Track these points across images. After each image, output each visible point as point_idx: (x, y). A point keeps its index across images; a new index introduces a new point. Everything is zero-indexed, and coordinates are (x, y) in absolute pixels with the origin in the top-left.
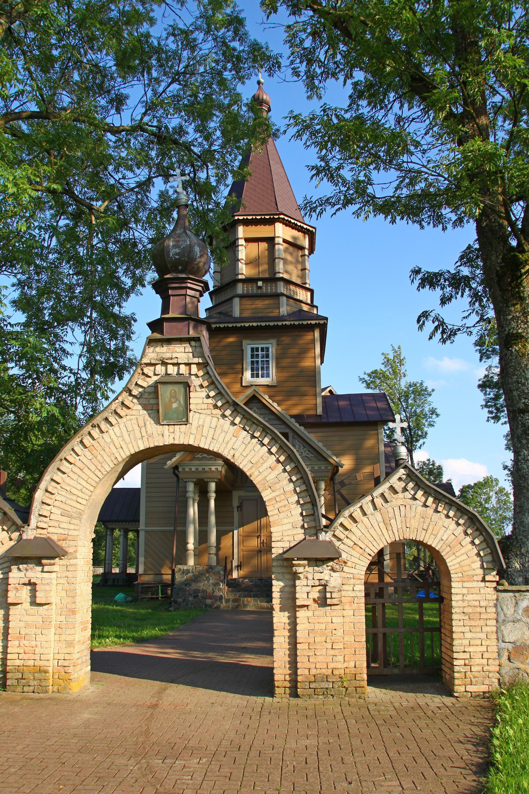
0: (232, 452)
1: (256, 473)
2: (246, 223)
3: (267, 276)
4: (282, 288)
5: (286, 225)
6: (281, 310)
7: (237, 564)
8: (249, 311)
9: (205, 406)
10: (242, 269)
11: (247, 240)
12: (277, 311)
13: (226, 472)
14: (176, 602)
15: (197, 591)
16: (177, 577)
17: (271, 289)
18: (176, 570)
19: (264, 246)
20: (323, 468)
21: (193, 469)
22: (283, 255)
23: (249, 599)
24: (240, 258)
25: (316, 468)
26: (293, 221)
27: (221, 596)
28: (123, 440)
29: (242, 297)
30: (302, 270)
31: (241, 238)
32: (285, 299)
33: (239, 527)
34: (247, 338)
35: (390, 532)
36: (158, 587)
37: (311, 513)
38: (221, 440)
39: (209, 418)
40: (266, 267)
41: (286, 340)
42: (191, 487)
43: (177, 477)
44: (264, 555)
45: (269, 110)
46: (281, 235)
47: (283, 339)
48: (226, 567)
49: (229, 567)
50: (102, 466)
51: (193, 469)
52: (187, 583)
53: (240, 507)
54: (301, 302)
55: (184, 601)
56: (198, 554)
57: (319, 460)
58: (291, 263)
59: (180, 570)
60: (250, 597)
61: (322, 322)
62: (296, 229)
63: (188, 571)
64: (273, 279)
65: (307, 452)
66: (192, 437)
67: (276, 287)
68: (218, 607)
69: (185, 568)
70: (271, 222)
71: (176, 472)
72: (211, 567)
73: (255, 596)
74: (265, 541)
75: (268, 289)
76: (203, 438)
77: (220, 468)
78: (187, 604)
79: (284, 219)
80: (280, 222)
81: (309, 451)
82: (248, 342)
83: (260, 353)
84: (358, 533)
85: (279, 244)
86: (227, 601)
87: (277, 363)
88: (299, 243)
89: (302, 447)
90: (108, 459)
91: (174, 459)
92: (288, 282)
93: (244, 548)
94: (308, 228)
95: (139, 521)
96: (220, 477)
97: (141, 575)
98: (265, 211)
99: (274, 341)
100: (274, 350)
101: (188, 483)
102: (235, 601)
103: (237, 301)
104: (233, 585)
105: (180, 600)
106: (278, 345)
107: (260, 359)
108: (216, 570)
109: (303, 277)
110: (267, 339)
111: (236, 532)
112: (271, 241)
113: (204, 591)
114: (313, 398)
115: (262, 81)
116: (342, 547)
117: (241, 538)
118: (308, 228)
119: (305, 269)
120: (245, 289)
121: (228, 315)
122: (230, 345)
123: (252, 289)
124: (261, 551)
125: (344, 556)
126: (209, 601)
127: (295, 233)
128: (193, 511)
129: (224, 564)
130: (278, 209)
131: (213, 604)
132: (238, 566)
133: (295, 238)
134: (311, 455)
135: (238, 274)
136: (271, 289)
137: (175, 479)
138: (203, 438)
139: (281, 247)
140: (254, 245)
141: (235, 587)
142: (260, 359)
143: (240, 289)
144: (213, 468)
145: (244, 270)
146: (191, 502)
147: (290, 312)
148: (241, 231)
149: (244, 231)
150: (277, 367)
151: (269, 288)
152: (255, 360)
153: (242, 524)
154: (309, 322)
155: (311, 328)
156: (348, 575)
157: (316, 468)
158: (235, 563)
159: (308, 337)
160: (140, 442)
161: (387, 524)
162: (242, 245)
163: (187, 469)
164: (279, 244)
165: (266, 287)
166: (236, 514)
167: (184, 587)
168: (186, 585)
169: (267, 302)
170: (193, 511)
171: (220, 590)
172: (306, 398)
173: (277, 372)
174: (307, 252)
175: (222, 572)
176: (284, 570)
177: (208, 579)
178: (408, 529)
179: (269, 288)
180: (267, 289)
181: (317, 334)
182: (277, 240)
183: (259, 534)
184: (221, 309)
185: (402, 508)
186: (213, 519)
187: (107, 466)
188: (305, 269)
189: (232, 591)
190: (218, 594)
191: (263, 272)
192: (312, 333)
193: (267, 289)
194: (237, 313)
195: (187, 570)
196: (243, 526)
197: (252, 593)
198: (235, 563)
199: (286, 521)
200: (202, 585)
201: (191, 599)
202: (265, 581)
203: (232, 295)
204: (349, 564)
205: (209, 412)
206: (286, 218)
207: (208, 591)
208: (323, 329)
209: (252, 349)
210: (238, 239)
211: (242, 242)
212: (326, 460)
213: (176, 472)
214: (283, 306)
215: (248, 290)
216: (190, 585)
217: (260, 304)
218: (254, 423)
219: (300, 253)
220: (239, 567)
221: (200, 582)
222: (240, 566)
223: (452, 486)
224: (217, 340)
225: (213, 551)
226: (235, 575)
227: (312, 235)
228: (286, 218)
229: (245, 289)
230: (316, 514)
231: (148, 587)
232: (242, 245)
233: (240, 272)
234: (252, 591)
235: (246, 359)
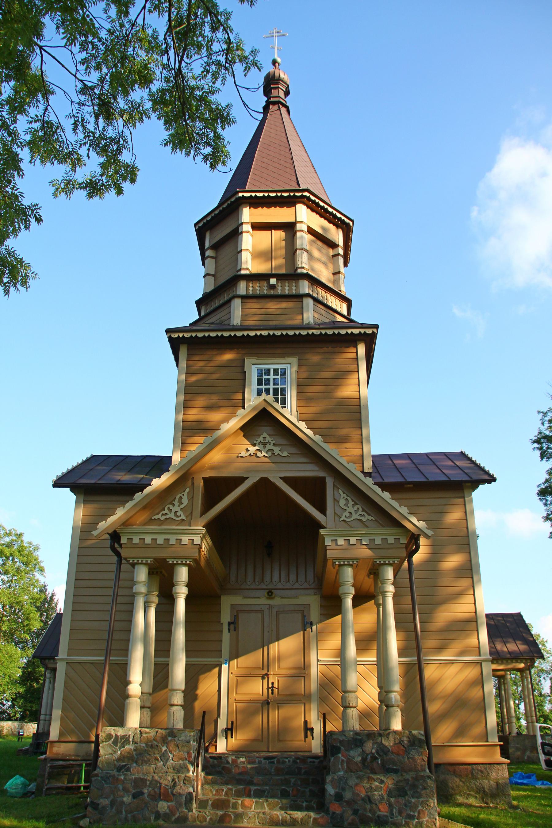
2: (255, 203)
3: (283, 271)
4: (305, 287)
5: (313, 210)
6: (305, 315)
7: (225, 726)
8: (256, 318)
10: (246, 262)
11: (256, 227)
12: (300, 317)
13: (209, 551)
14: (95, 806)
15: (140, 782)
16: (102, 751)
18: (102, 736)
19: (279, 235)
20: (391, 540)
21: (148, 540)
22: (307, 246)
23: (247, 801)
24: (244, 247)
25: (378, 540)
26: (322, 204)
27: (190, 794)
29: (243, 297)
30: (334, 274)
31: (247, 223)
32: (310, 301)
33: (231, 658)
34: (251, 355)
36: (81, 765)
40: (282, 261)
41: (314, 358)
42: (142, 574)
43: (118, 554)
44: (274, 709)
45: (287, 93)
46: (305, 220)
47: (309, 356)
48: (202, 731)
49: (209, 730)
51: (148, 540)
52: (123, 765)
53: (233, 624)
54: (335, 311)
55: (112, 803)
56: (154, 706)
57: (383, 526)
58: (319, 260)
59: (109, 736)
60: (249, 796)
61: (369, 331)
62: (325, 219)
63: (125, 740)
64: (294, 275)
65: (360, 512)
67: (297, 287)
68: (183, 819)
69: (120, 732)
70: (289, 202)
71: (116, 545)
72: (172, 733)
73: (259, 794)
74: (276, 685)
75: (286, 289)
77: (197, 540)
78: (119, 812)
79: (308, 198)
80: (304, 204)
81: (363, 510)
82: (254, 360)
83: (272, 377)
85: (302, 231)
86: (203, 804)
87: (299, 393)
88: (329, 237)
89: (351, 503)
91: (112, 519)
92: (315, 282)
93: (238, 697)
94: (343, 218)
95: (155, 664)
96: (196, 555)
97: (53, 742)
98: (281, 185)
99: (294, 360)
100: (294, 375)
101: (136, 567)
102: (219, 804)
103: (237, 303)
104: (216, 767)
105: (104, 802)
106: (300, 365)
107: (271, 387)
108: (182, 738)
109: (336, 282)
110: (283, 356)
111: (224, 667)
112: (289, 228)
113: (155, 784)
114: (358, 445)
115: (279, 60)
117: (233, 678)
118: (343, 218)
119: (339, 273)
120: (251, 289)
121: (225, 326)
122: (228, 365)
124: (268, 703)
126: (163, 806)
127: (325, 223)
128: (144, 619)
129: (201, 724)
130: (298, 184)
131: (172, 812)
132: (226, 730)
133: (324, 229)
134: (368, 517)
135: (241, 270)
137: (115, 559)
139: (303, 239)
140: (265, 235)
141: (219, 773)
142: (271, 387)
143: (242, 288)
144: (185, 540)
145: (249, 263)
146: (140, 603)
147: (319, 322)
148: (247, 214)
149: (250, 215)
150: (299, 399)
151: (287, 288)
152: (264, 387)
153: (235, 655)
154: (349, 331)
155: (351, 341)
157: (378, 540)
158: (222, 724)
159: (350, 353)
162: (247, 232)
163: (136, 541)
164: (302, 231)
166: (226, 636)
167: (115, 772)
168: (119, 769)
169: (284, 305)
170: (144, 619)
171: (187, 781)
172: (348, 445)
173: (298, 406)
175: (194, 744)
177: (164, 757)
179: (287, 288)
181: (361, 349)
182: (298, 226)
183: (265, 672)
184: (213, 319)
186: (180, 635)
188: (339, 273)
189: (213, 783)
190: (183, 789)
191: (280, 267)
192: (353, 350)
194: (237, 319)
195: (123, 737)
196: (237, 657)
197: (253, 788)
198: (222, 724)
200: (151, 771)
201: (127, 799)
202: (278, 762)
203: (230, 296)
206: (313, 198)
207: (163, 782)
208: (370, 340)
210: (242, 224)
211: (247, 227)
212: (400, 525)
213: (116, 545)
214: (308, 311)
216: (128, 770)
217: (273, 307)
219: (331, 252)
220: (229, 731)
221: (148, 762)
222: (231, 730)
223: (522, 617)
224: (205, 357)
225: (178, 699)
226: (221, 747)
227: (346, 228)
228: (313, 198)
229: (251, 289)
231: (63, 767)
232: (247, 232)
233: (243, 266)
234: (251, 783)
235: (250, 385)
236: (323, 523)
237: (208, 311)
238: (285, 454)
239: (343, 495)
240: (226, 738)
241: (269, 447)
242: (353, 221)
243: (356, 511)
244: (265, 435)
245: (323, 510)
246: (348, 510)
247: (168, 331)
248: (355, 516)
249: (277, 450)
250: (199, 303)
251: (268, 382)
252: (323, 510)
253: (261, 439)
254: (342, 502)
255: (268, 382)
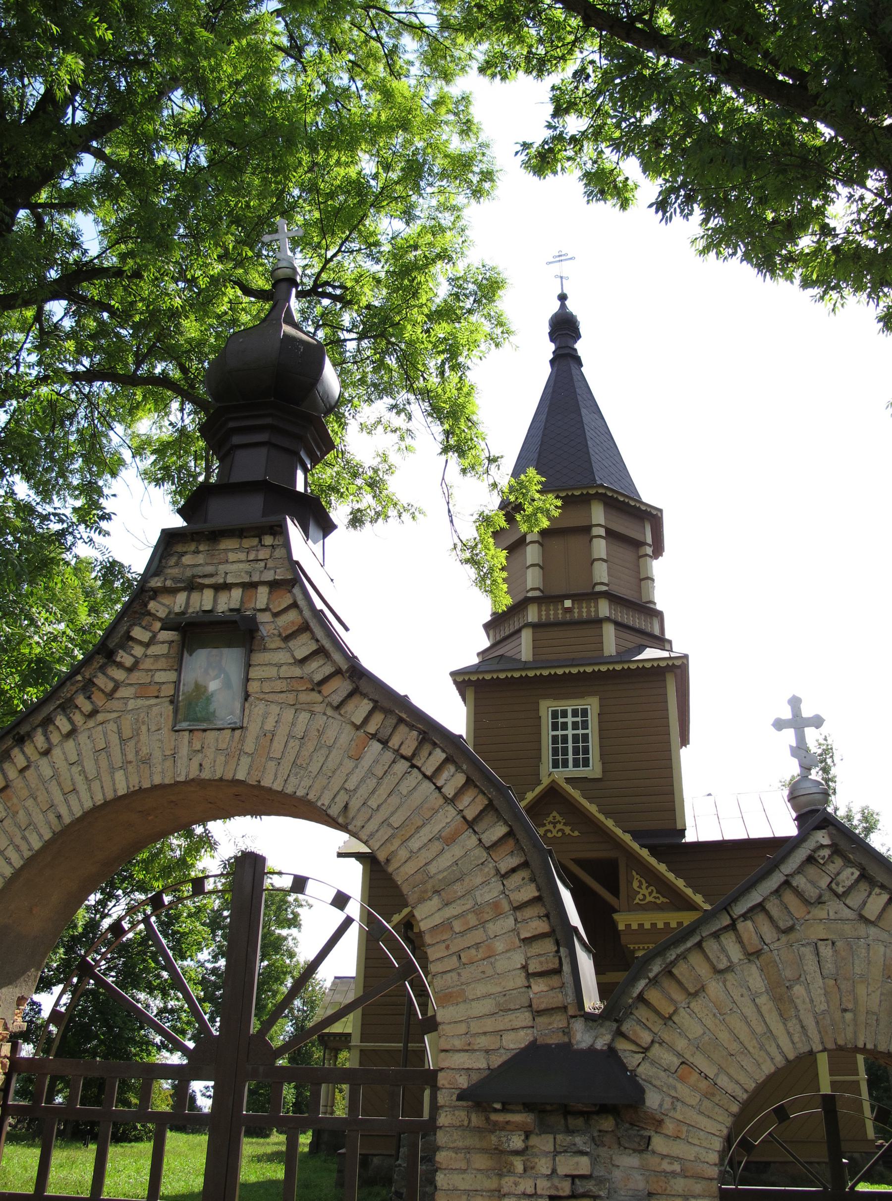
0: (342, 798)
1: (403, 854)
9: (280, 685)
17: (589, 612)
28: (83, 772)
29: (534, 626)
35: (793, 1025)
37: (551, 966)
38: (314, 768)
39: (289, 714)
50: (24, 838)
65: (654, 894)
66: (245, 761)
67: (596, 607)
75: (583, 612)
76: (272, 765)
84: (695, 1030)
89: (645, 885)
90: (38, 818)
107: (570, 732)
110: (582, 695)
116: (645, 1071)
123: (556, 614)
125: (653, 1100)
134: (662, 899)
136: (589, 612)
138: (272, 765)
142: (570, 732)
151: (584, 610)
156: (666, 1166)
160: (119, 776)
161: (781, 995)
165: (580, 608)
174: (649, 550)
176: (471, 1141)
178: (849, 1016)
180: (580, 612)
185: (826, 951)
187: (35, 835)
193: (580, 612)
199: (480, 989)
204: (669, 1127)
205: (291, 698)
209: (555, 715)
215: (548, 615)
218: (401, 720)
229: (544, 613)
230: (566, 968)
236: (616, 907)
237: (498, 639)
238: (576, 833)
239: (636, 876)
240: (222, 875)
241: (559, 826)
242: (661, 511)
243: (650, 894)
244: (555, 814)
245: (616, 892)
246: (642, 892)
247: (453, 674)
248: (649, 899)
249: (567, 830)
250: (487, 627)
251: (564, 726)
252: (616, 892)
253: (550, 819)
254: (635, 884)
255: (564, 726)
